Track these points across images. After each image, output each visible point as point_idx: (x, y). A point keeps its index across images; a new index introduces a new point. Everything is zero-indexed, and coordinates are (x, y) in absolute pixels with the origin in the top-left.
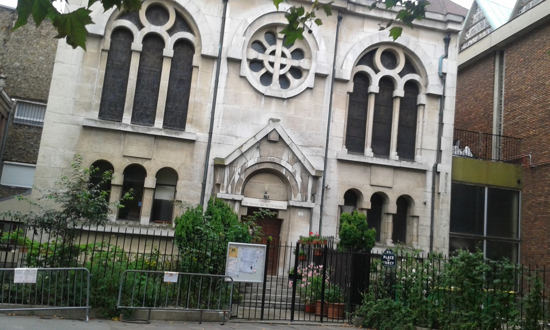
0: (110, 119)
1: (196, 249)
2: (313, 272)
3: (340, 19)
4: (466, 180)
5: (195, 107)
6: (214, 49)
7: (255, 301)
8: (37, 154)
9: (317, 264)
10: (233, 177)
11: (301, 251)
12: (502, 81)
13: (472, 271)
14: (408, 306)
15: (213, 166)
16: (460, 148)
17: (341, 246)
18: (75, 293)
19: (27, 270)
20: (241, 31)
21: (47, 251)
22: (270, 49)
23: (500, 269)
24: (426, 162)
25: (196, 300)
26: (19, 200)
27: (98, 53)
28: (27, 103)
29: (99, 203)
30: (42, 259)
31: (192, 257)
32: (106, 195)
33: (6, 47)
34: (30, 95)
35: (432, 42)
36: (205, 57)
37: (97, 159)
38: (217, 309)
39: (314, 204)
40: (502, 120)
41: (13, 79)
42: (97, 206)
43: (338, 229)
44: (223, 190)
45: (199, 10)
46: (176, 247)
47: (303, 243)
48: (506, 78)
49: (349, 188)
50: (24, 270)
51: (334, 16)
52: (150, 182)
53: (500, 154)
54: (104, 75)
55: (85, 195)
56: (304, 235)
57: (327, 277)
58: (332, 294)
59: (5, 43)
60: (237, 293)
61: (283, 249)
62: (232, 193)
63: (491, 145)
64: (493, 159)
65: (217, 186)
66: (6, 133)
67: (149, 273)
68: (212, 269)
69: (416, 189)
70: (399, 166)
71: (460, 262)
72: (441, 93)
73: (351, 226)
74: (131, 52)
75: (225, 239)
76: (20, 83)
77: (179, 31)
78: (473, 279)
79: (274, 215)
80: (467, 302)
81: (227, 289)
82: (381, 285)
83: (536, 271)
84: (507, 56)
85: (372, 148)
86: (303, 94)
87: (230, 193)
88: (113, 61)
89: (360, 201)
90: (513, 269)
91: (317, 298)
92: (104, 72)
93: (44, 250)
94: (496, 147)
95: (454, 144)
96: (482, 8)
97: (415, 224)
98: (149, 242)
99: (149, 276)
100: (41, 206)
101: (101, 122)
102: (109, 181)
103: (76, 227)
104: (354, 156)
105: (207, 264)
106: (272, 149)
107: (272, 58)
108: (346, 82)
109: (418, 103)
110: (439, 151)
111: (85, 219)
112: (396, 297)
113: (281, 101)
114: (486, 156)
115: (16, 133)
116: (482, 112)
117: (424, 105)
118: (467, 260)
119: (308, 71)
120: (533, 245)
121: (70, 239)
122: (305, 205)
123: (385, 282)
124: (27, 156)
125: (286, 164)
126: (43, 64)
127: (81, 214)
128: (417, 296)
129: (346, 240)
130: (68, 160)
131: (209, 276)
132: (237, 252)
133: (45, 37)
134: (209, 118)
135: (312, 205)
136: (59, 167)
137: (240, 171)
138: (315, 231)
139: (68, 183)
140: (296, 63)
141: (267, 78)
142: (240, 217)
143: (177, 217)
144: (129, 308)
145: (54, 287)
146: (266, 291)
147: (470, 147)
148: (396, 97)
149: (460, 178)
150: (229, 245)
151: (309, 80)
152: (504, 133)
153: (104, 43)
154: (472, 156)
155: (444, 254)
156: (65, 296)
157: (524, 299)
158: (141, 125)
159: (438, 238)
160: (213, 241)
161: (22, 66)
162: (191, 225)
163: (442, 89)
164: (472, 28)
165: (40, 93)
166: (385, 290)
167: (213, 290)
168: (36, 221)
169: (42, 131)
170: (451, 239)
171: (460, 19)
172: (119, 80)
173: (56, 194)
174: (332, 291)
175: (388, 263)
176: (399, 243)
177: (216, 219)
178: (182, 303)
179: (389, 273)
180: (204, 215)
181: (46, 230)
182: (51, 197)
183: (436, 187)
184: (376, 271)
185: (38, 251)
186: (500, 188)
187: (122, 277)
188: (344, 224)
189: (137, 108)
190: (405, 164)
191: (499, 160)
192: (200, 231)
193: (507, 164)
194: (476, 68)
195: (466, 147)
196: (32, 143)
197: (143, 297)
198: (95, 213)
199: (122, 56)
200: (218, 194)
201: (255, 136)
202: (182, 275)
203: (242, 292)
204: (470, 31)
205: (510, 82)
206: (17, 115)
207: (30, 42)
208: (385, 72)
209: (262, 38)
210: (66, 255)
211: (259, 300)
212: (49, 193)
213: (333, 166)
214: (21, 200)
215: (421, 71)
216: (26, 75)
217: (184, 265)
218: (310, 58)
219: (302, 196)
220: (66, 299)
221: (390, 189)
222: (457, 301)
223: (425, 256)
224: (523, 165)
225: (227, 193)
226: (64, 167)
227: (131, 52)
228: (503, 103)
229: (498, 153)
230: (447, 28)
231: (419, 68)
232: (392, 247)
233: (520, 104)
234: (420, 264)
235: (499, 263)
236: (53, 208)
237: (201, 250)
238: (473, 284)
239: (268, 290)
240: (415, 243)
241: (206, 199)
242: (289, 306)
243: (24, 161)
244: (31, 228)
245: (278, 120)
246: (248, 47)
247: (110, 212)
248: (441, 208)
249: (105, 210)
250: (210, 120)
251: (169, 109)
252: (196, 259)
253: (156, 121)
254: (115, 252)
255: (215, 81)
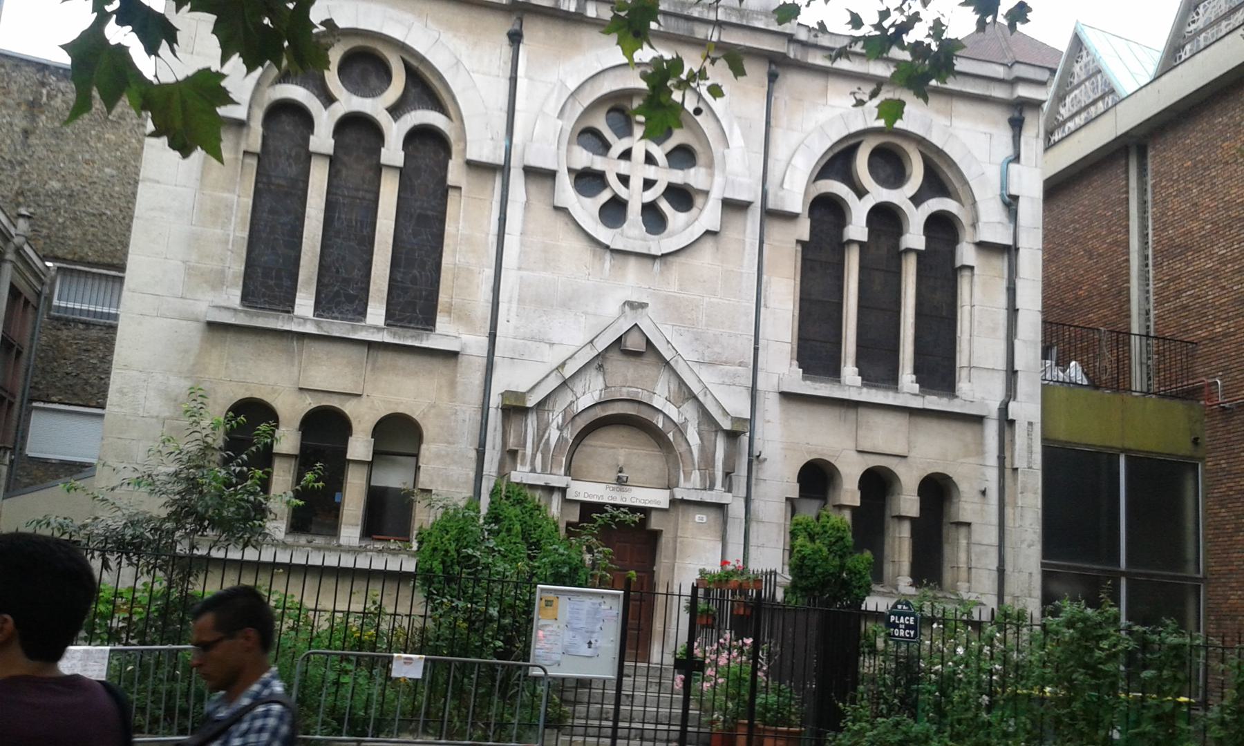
0: (267, 306)
1: (464, 601)
2: (730, 653)
3: (773, 78)
4: (1075, 439)
5: (455, 277)
6: (495, 148)
7: (596, 723)
8: (107, 385)
9: (739, 636)
10: (547, 435)
11: (702, 604)
12: (1145, 212)
13: (1092, 651)
14: (946, 734)
15: (500, 410)
16: (1057, 365)
17: (794, 593)
18: (192, 702)
19: (86, 652)
20: (553, 107)
21: (132, 608)
22: (619, 146)
23: (1156, 647)
24: (983, 398)
25: (463, 720)
26: (68, 490)
27: (237, 159)
28: (80, 271)
29: (245, 497)
30: (121, 625)
31: (456, 619)
32: (260, 479)
33: (29, 146)
34: (87, 254)
35: (982, 127)
36: (474, 166)
37: (240, 397)
38: (511, 741)
39: (730, 495)
40: (1152, 299)
41: (47, 219)
42: (243, 503)
43: (787, 553)
44: (523, 464)
45: (458, 62)
46: (420, 597)
47: (708, 586)
48: (1155, 204)
49: (809, 458)
50: (78, 651)
51: (756, 72)
52: (359, 447)
53: (1149, 379)
54: (250, 209)
55: (215, 478)
56: (708, 568)
57: (762, 666)
58: (772, 705)
59: (27, 138)
60: (556, 705)
61: (660, 600)
62: (544, 470)
63: (1130, 359)
64: (1133, 389)
65: (511, 455)
66: (36, 338)
67: (358, 657)
68: (500, 647)
69: (963, 460)
70: (920, 406)
71: (1065, 630)
72: (1009, 242)
73: (816, 547)
74: (309, 156)
75: (531, 577)
76: (64, 227)
77: (415, 109)
78: (1093, 670)
79: (637, 520)
80: (1081, 725)
81: (533, 694)
82: (885, 685)
83: (1237, 651)
84: (1154, 156)
85: (857, 366)
86: (697, 246)
87: (539, 470)
88: (269, 176)
89: (834, 489)
90: (1185, 645)
91: (737, 716)
92: (249, 201)
93: (124, 604)
94: (1141, 364)
95: (1045, 355)
96: (1092, 50)
97: (963, 542)
98: (360, 585)
99: (358, 664)
100: (118, 503)
101: (245, 312)
102: (269, 447)
103: (195, 552)
104: (817, 385)
105: (488, 636)
106: (631, 370)
107: (624, 167)
108: (792, 217)
109: (958, 264)
110: (1011, 373)
111: (217, 532)
112: (920, 711)
113: (648, 262)
114: (1119, 383)
115: (58, 339)
116: (1104, 283)
117: (972, 268)
118: (1080, 625)
119: (706, 193)
120: (1232, 588)
121: (183, 579)
122: (708, 497)
123: (895, 677)
124: (84, 390)
125: (665, 405)
126: (114, 185)
127: (206, 523)
128: (967, 710)
129: (806, 578)
130: (176, 400)
131: (494, 664)
132: (557, 608)
133: (117, 125)
134: (487, 301)
135: (726, 498)
136: (155, 414)
137: (560, 422)
138: (735, 556)
139: (177, 452)
140: (678, 177)
141: (614, 211)
142: (564, 525)
143: (421, 527)
144: (312, 740)
145: (145, 690)
146: (623, 698)
147: (1081, 362)
148: (908, 250)
149: (1062, 434)
150: (538, 590)
151: (709, 215)
152: (1156, 330)
153: (248, 135)
154: (1085, 382)
155: (1029, 611)
156: (169, 712)
157: (1209, 715)
158: (336, 318)
159: (1016, 574)
160: (502, 582)
161: (66, 188)
162: (454, 545)
163: (1012, 231)
164: (1072, 95)
165: (108, 248)
166: (895, 696)
167: (503, 696)
168: (107, 538)
169: (115, 334)
170: (1047, 576)
171: (1043, 75)
172: (284, 219)
173: (149, 476)
174: (772, 698)
175: (902, 634)
176: (927, 585)
177: (509, 530)
178: (432, 728)
179: (904, 658)
180: (482, 521)
181: (129, 558)
182: (139, 484)
183: (1008, 454)
184: (873, 651)
185: (111, 607)
186: (1154, 456)
187: (298, 666)
188: (800, 541)
189: (326, 281)
190: (934, 402)
191: (1148, 393)
192: (474, 560)
193: (1166, 401)
194: (1085, 183)
195: (1073, 363)
196: (95, 361)
197: (344, 714)
198: (238, 520)
199: (290, 165)
200: (513, 472)
201: (591, 342)
202: (433, 661)
203: (567, 702)
204: (1068, 100)
205: (1163, 214)
206: (59, 299)
207: (83, 135)
208: (879, 194)
209: (600, 123)
210: (174, 616)
211: (607, 719)
212: (136, 475)
213: (771, 407)
214: (72, 491)
215: (960, 192)
216: (76, 208)
217: (438, 638)
218: (710, 165)
219: (703, 478)
220: (172, 719)
221: (903, 460)
222: (1058, 721)
223: (986, 617)
224: (1202, 402)
225: (533, 470)
226: (167, 414)
227: (309, 156)
228: (1150, 262)
229: (1145, 376)
230: (1015, 96)
231: (958, 185)
232: (911, 596)
233: (1188, 264)
234: (975, 636)
235: (1153, 632)
236: (144, 508)
237: (476, 603)
238: (1093, 682)
239: (627, 696)
240: (962, 586)
241: (487, 486)
242: (674, 735)
243: (77, 402)
244: (97, 553)
245: (643, 306)
246: (570, 143)
247: (272, 516)
248: (1020, 504)
249: (261, 511)
250: (490, 305)
251: (398, 282)
252: (465, 625)
253: (369, 310)
254: (284, 608)
255: (499, 219)
